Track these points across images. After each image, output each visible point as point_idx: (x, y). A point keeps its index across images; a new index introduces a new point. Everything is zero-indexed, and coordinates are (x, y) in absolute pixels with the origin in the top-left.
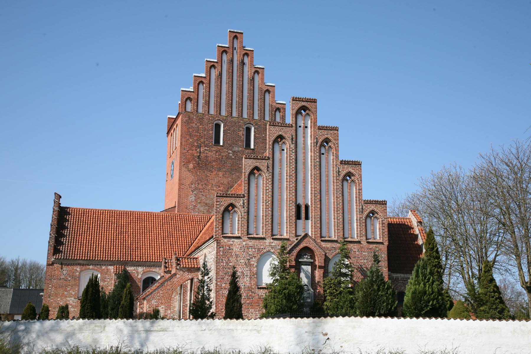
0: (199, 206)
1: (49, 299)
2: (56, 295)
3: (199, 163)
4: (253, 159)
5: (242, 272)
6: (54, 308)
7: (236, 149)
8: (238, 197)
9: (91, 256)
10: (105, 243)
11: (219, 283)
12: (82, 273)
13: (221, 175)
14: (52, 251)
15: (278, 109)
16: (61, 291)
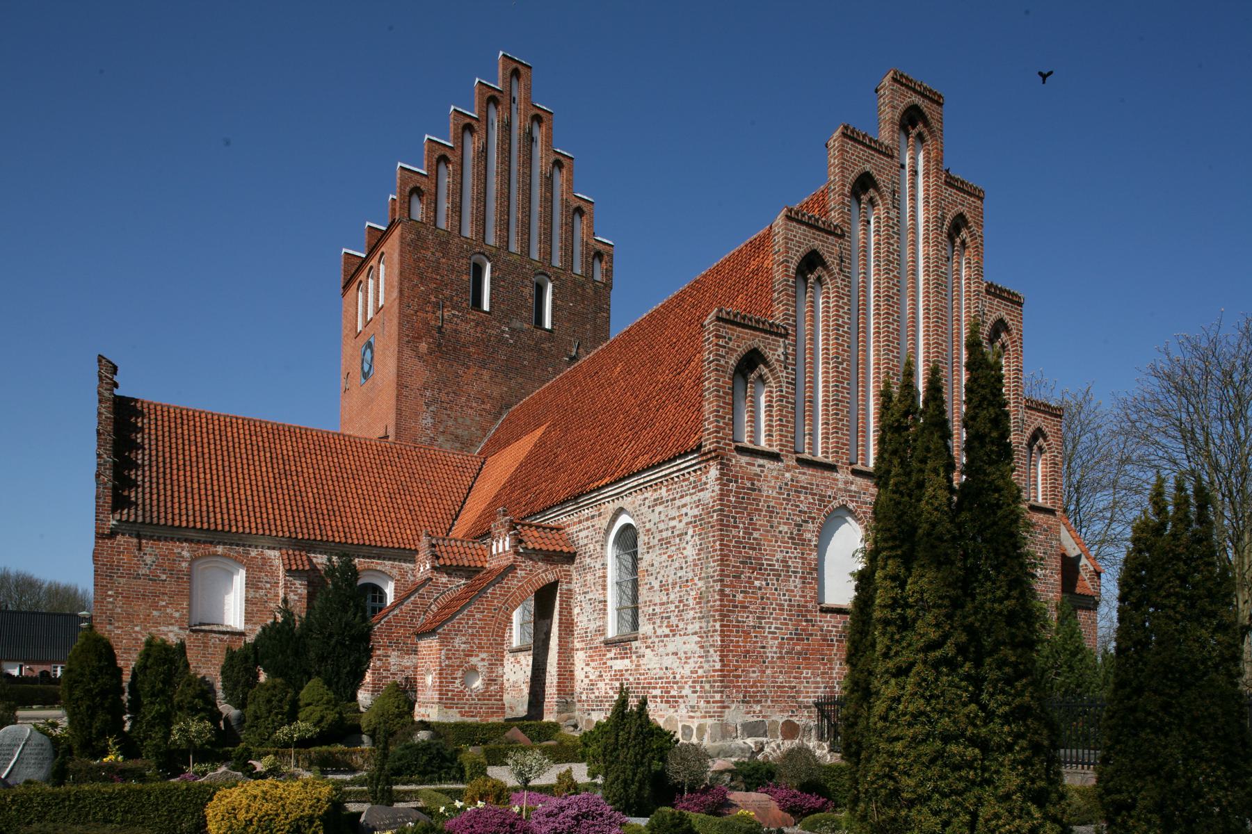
0: (441, 439)
1: (108, 627)
2: (130, 618)
3: (440, 344)
4: (807, 225)
5: (784, 561)
6: (127, 650)
7: (517, 324)
8: (771, 333)
9: (219, 521)
10: (249, 492)
11: (727, 591)
12: (197, 563)
13: (486, 377)
14: (109, 500)
15: (599, 255)
16: (141, 608)
